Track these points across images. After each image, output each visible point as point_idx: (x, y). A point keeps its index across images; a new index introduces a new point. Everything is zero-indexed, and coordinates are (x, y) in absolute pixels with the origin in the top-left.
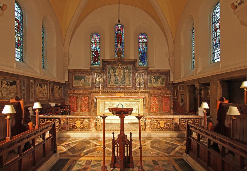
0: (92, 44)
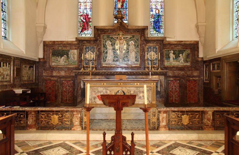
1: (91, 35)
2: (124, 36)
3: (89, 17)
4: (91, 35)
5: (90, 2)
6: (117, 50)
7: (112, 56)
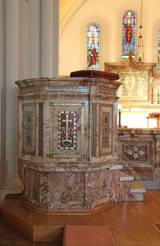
2: (134, 72)
3: (97, 52)
5: (98, 37)
6: (127, 85)
7: (122, 91)
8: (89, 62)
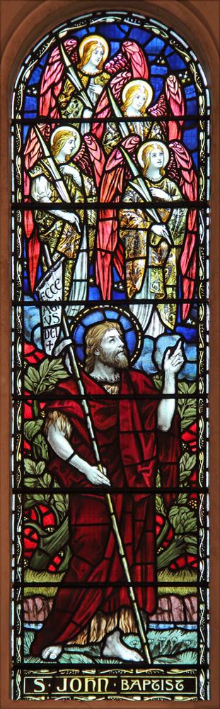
0: (37, 236)
1: (189, 685)
4: (189, 685)
8: (45, 578)
